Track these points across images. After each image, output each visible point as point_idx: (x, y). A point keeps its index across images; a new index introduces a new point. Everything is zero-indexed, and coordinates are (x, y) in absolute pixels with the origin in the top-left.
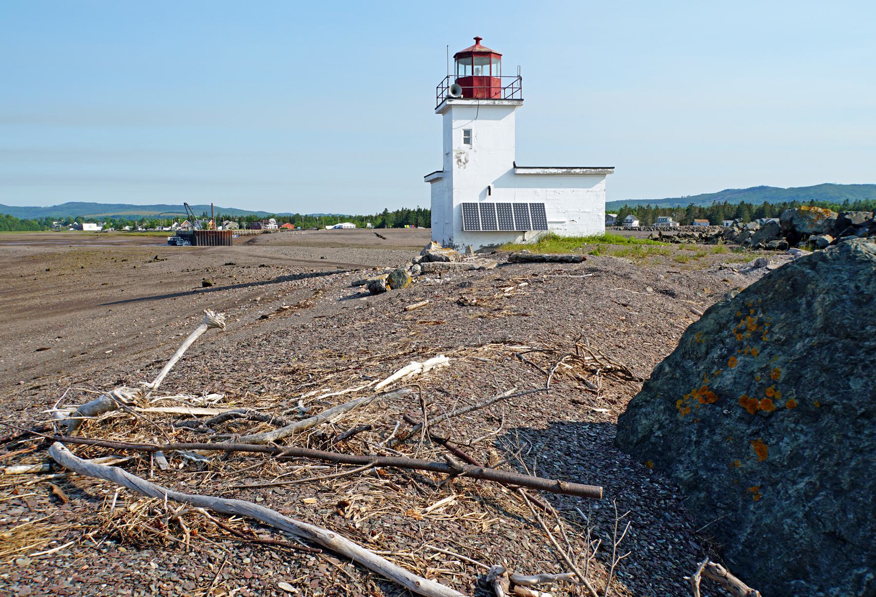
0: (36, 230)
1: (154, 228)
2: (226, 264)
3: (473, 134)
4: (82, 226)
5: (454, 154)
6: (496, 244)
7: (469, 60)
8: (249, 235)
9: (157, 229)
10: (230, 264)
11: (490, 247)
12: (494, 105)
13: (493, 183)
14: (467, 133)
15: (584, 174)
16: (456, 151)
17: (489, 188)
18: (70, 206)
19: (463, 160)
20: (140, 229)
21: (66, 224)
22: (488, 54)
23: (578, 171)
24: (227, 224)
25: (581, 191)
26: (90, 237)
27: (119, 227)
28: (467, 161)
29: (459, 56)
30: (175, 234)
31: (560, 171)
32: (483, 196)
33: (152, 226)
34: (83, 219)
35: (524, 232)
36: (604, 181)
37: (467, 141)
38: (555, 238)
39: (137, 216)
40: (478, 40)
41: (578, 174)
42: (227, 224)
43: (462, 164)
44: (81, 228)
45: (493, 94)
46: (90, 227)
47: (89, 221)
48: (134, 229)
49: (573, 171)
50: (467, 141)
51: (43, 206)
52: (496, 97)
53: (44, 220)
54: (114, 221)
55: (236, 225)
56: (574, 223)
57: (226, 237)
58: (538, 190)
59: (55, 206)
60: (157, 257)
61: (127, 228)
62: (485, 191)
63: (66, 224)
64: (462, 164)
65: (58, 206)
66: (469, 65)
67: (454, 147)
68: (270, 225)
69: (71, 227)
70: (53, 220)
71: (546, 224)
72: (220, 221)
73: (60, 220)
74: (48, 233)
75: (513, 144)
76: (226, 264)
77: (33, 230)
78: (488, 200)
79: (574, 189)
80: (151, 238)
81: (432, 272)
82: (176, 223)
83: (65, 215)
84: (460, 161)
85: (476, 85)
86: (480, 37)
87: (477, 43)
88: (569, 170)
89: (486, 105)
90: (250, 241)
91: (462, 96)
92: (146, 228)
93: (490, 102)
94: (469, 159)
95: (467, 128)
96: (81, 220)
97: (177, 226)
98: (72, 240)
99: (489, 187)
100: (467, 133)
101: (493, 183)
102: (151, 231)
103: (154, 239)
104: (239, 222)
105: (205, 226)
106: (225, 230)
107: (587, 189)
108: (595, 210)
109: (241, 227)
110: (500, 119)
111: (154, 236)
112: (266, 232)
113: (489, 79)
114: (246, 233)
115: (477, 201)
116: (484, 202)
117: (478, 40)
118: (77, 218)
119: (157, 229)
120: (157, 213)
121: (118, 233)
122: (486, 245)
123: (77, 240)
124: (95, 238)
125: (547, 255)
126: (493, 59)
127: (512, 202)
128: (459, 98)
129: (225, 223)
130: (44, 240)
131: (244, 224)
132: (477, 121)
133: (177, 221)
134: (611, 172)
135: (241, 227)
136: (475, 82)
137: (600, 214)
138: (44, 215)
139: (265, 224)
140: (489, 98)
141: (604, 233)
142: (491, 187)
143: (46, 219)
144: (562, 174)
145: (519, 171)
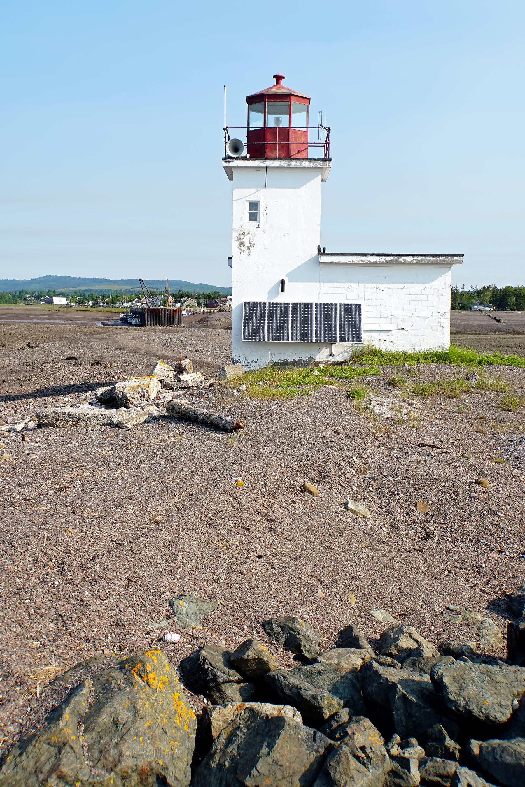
0: (9, 303)
1: (115, 303)
2: (68, 359)
3: (262, 207)
4: (53, 299)
5: (235, 235)
6: (291, 359)
7: (260, 106)
8: (203, 313)
9: (118, 304)
10: (72, 358)
11: (282, 364)
12: (289, 168)
13: (286, 276)
14: (253, 206)
15: (419, 264)
16: (237, 231)
17: (283, 282)
18: (47, 279)
19: (247, 244)
20: (101, 304)
21: (38, 297)
22: (287, 97)
23: (409, 259)
24: (186, 301)
25: (416, 288)
26: (48, 312)
27: (81, 302)
28: (252, 245)
29: (252, 100)
30: (129, 310)
31: (383, 259)
32: (272, 293)
33: (113, 302)
34: (54, 292)
35: (332, 344)
36: (449, 274)
37: (253, 217)
38: (375, 353)
39: (109, 290)
40: (278, 78)
41: (409, 263)
42: (186, 301)
43: (245, 248)
44: (51, 302)
45: (292, 153)
46: (60, 301)
47: (59, 295)
48: (96, 304)
49: (402, 259)
50: (253, 217)
51: (21, 279)
52: (298, 156)
53: (18, 293)
54: (84, 295)
55: (194, 302)
56: (404, 332)
57: (176, 315)
58: (353, 285)
59: (32, 279)
60: (29, 343)
61: (90, 303)
62: (277, 285)
63: (38, 297)
64: (245, 248)
65: (36, 279)
66: (285, 113)
67: (236, 225)
68: (227, 303)
69: (42, 301)
70: (27, 293)
71: (360, 334)
72: (179, 297)
73: (33, 293)
74: (20, 307)
75: (319, 222)
76: (68, 359)
77: (6, 303)
78: (281, 298)
79: (406, 285)
80: (107, 315)
81: (53, 425)
82: (136, 299)
83: (37, 288)
84: (242, 244)
85: (269, 141)
86: (281, 74)
87: (277, 83)
88: (396, 258)
89: (278, 167)
90: (202, 320)
91: (248, 156)
92: (108, 304)
93: (284, 163)
94: (256, 241)
95: (253, 199)
96: (52, 294)
97: (137, 302)
98: (32, 315)
99: (283, 280)
100: (253, 206)
101: (286, 276)
102: (112, 307)
103: (110, 315)
104: (198, 299)
105: (164, 303)
106: (175, 308)
107: (424, 286)
108: (436, 314)
109: (199, 305)
110: (299, 188)
111: (111, 312)
112: (222, 311)
113: (286, 133)
114: (201, 311)
115: (263, 298)
116: (275, 301)
117: (278, 78)
118: (49, 292)
119: (118, 304)
120: (128, 287)
121: (80, 308)
122: (276, 360)
123: (36, 315)
124: (53, 314)
125: (205, 410)
126: (294, 104)
127: (338, 302)
128: (244, 158)
129: (183, 300)
130: (5, 314)
131: (202, 301)
132: (268, 190)
133: (138, 298)
134: (458, 262)
135: (199, 305)
136: (268, 136)
137: (442, 320)
138: (20, 289)
139: (223, 301)
140: (288, 157)
141: (448, 349)
142: (286, 282)
143: (20, 292)
144: (387, 263)
145: (324, 259)
